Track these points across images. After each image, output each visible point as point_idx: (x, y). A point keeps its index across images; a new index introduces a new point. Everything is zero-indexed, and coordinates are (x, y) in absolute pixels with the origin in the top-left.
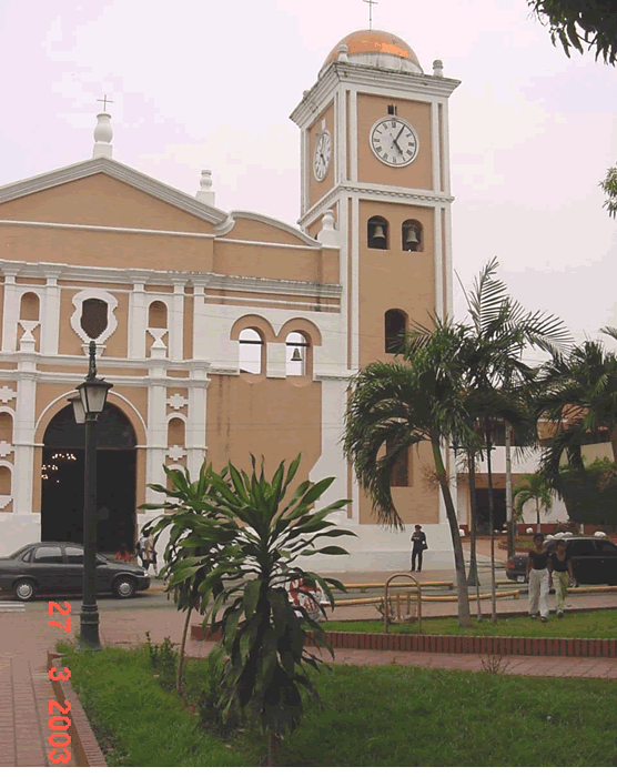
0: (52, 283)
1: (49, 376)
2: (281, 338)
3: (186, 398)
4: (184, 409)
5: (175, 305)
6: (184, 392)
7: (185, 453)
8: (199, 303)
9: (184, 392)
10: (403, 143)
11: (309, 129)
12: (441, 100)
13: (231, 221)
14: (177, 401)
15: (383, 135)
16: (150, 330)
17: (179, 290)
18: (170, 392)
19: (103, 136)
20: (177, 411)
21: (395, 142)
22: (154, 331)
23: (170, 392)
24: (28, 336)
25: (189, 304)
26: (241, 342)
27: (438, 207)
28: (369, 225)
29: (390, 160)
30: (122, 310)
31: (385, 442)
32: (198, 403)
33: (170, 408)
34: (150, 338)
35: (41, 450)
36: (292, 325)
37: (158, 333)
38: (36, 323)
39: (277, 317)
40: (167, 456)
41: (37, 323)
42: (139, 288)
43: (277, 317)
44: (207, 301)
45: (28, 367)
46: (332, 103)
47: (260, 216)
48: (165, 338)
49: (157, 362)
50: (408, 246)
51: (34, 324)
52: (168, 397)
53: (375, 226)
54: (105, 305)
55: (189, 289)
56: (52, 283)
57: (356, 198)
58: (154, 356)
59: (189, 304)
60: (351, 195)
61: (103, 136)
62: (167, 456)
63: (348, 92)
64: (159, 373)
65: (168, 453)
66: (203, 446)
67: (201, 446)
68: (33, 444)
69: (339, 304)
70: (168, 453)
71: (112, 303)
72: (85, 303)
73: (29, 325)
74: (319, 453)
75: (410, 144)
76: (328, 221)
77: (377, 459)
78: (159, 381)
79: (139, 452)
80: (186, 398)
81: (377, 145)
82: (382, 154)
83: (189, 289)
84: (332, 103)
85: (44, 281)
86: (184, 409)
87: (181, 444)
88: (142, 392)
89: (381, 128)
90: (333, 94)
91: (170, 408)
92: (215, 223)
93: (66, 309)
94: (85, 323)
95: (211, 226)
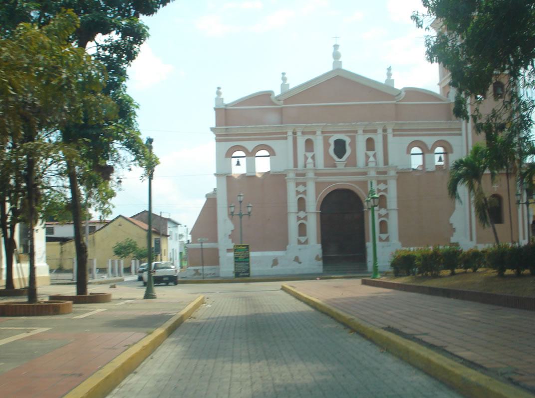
0: (319, 133)
1: (322, 179)
5: (378, 139)
7: (306, 214)
14: (301, 188)
23: (379, 182)
25: (385, 138)
37: (371, 153)
44: (394, 135)
59: (385, 138)
64: (373, 173)
71: (348, 140)
83: (385, 130)
93: (326, 145)
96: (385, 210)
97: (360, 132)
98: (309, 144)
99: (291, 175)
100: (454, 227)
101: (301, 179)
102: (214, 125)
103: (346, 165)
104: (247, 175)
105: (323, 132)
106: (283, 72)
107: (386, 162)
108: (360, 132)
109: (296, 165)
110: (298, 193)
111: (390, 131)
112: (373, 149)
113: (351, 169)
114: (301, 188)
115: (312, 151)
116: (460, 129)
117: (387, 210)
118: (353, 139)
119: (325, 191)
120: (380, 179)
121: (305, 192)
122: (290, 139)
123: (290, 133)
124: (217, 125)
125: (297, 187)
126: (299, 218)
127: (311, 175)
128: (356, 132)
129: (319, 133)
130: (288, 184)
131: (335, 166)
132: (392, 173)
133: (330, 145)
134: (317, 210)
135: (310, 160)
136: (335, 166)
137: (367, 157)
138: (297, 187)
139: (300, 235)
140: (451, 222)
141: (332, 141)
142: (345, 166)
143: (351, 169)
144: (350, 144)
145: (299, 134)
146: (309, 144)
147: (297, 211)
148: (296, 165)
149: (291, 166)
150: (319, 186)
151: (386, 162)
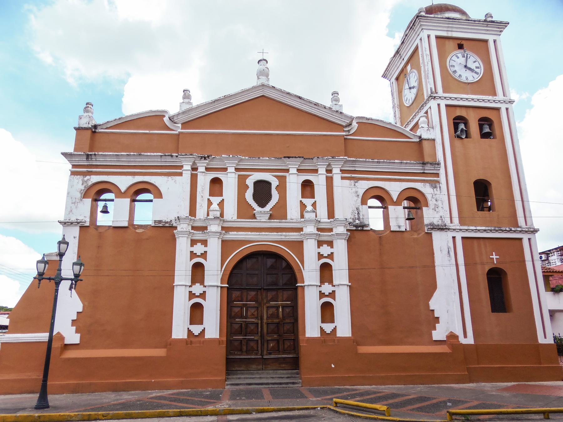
0: (231, 170)
1: (232, 236)
2: (397, 203)
3: (332, 247)
4: (331, 256)
5: (319, 181)
6: (330, 244)
7: (333, 289)
9: (330, 244)
12: (495, 37)
14: (325, 250)
18: (320, 244)
19: (264, 73)
20: (326, 257)
21: (466, 66)
22: (305, 201)
23: (320, 244)
25: (330, 181)
26: (370, 207)
27: (503, 107)
30: (282, 188)
31: (332, 365)
33: (320, 256)
35: (226, 289)
37: (308, 202)
40: (320, 292)
44: (343, 178)
45: (214, 227)
46: (417, 48)
48: (314, 205)
49: (310, 221)
50: (485, 136)
51: (219, 199)
53: (459, 123)
55: (329, 171)
57: (443, 103)
58: (307, 216)
59: (330, 181)
60: (439, 101)
62: (320, 292)
63: (429, 37)
64: (310, 229)
65: (191, 289)
66: (347, 283)
68: (219, 284)
69: (438, 177)
70: (191, 289)
71: (275, 183)
75: (475, 62)
76: (424, 123)
77: (54, 335)
79: (299, 290)
80: (332, 247)
81: (453, 69)
82: (457, 75)
83: (329, 171)
84: (417, 48)
85: (225, 169)
86: (331, 256)
87: (331, 282)
88: (298, 246)
89: (454, 58)
90: (418, 41)
91: (320, 256)
92: (344, 124)
93: (242, 187)
94: (256, 197)
95: (340, 127)
96: (202, 286)
97: (293, 171)
98: (216, 183)
99: (183, 227)
100: (436, 316)
101: (199, 235)
102: (70, 149)
103: (271, 217)
104: (152, 225)
105: (237, 170)
106: (185, 88)
107: (331, 214)
108: (293, 171)
109: (193, 211)
110: (193, 255)
111: (336, 171)
112: (312, 196)
113: (275, 224)
114: (199, 249)
115: (313, 197)
116: (437, 175)
117: (205, 287)
118: (283, 181)
119: (235, 255)
120: (322, 239)
121: (204, 255)
122: (187, 175)
123: (187, 167)
124: (75, 150)
125: (319, 247)
126: (192, 295)
127: (214, 227)
128: (287, 171)
129: (231, 170)
130: (178, 241)
131: (254, 217)
132: (341, 230)
133: (247, 187)
134: (222, 282)
135: (215, 206)
136: (254, 217)
137: (303, 206)
138: (319, 247)
139: (323, 321)
140: (431, 308)
141: (250, 182)
142: (270, 219)
143: (275, 224)
144: (277, 188)
145: (201, 169)
146: (216, 183)
147: (190, 284)
148: (193, 211)
149: (185, 212)
150: (227, 246)
151: (331, 214)
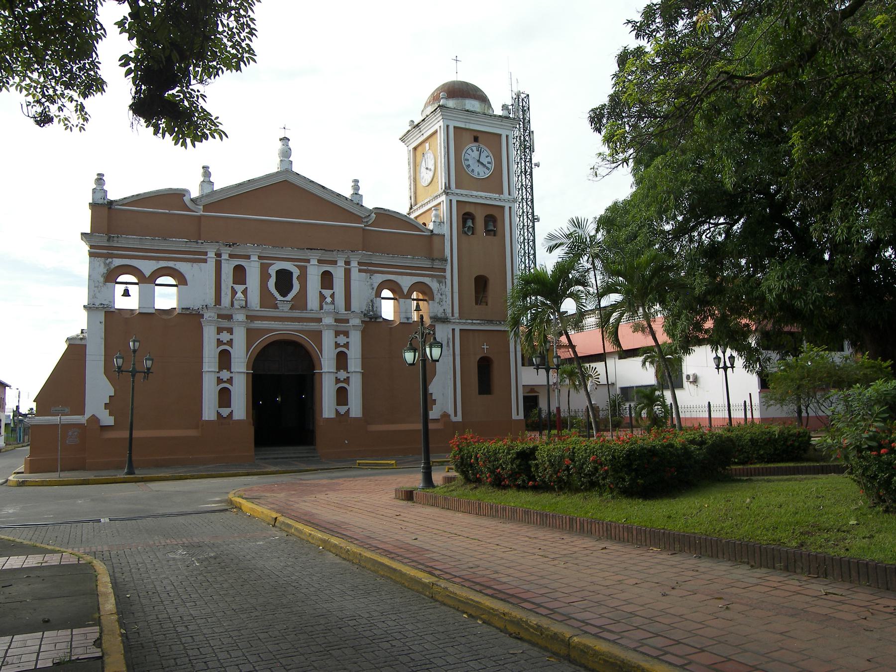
0: (254, 258)
1: (258, 324)
5: (338, 274)
6: (346, 334)
8: (355, 273)
10: (484, 160)
11: (415, 149)
13: (373, 215)
15: (471, 153)
16: (235, 286)
17: (341, 263)
18: (337, 334)
19: (286, 153)
20: (342, 346)
21: (479, 161)
22: (237, 287)
24: (239, 295)
25: (348, 273)
28: (463, 218)
29: (482, 174)
30: (303, 278)
32: (355, 340)
34: (234, 292)
35: (251, 375)
36: (415, 287)
38: (244, 287)
39: (406, 282)
41: (244, 287)
42: (314, 262)
43: (406, 282)
44: (360, 271)
47: (177, 189)
51: (243, 287)
52: (336, 337)
54: (291, 274)
55: (347, 263)
56: (254, 258)
59: (348, 273)
61: (286, 153)
62: (336, 377)
65: (218, 375)
67: (213, 370)
71: (296, 272)
72: (277, 272)
73: (239, 288)
74: (105, 373)
78: (328, 326)
80: (348, 337)
82: (470, 169)
83: (347, 263)
87: (229, 368)
89: (469, 151)
91: (337, 345)
95: (358, 219)
